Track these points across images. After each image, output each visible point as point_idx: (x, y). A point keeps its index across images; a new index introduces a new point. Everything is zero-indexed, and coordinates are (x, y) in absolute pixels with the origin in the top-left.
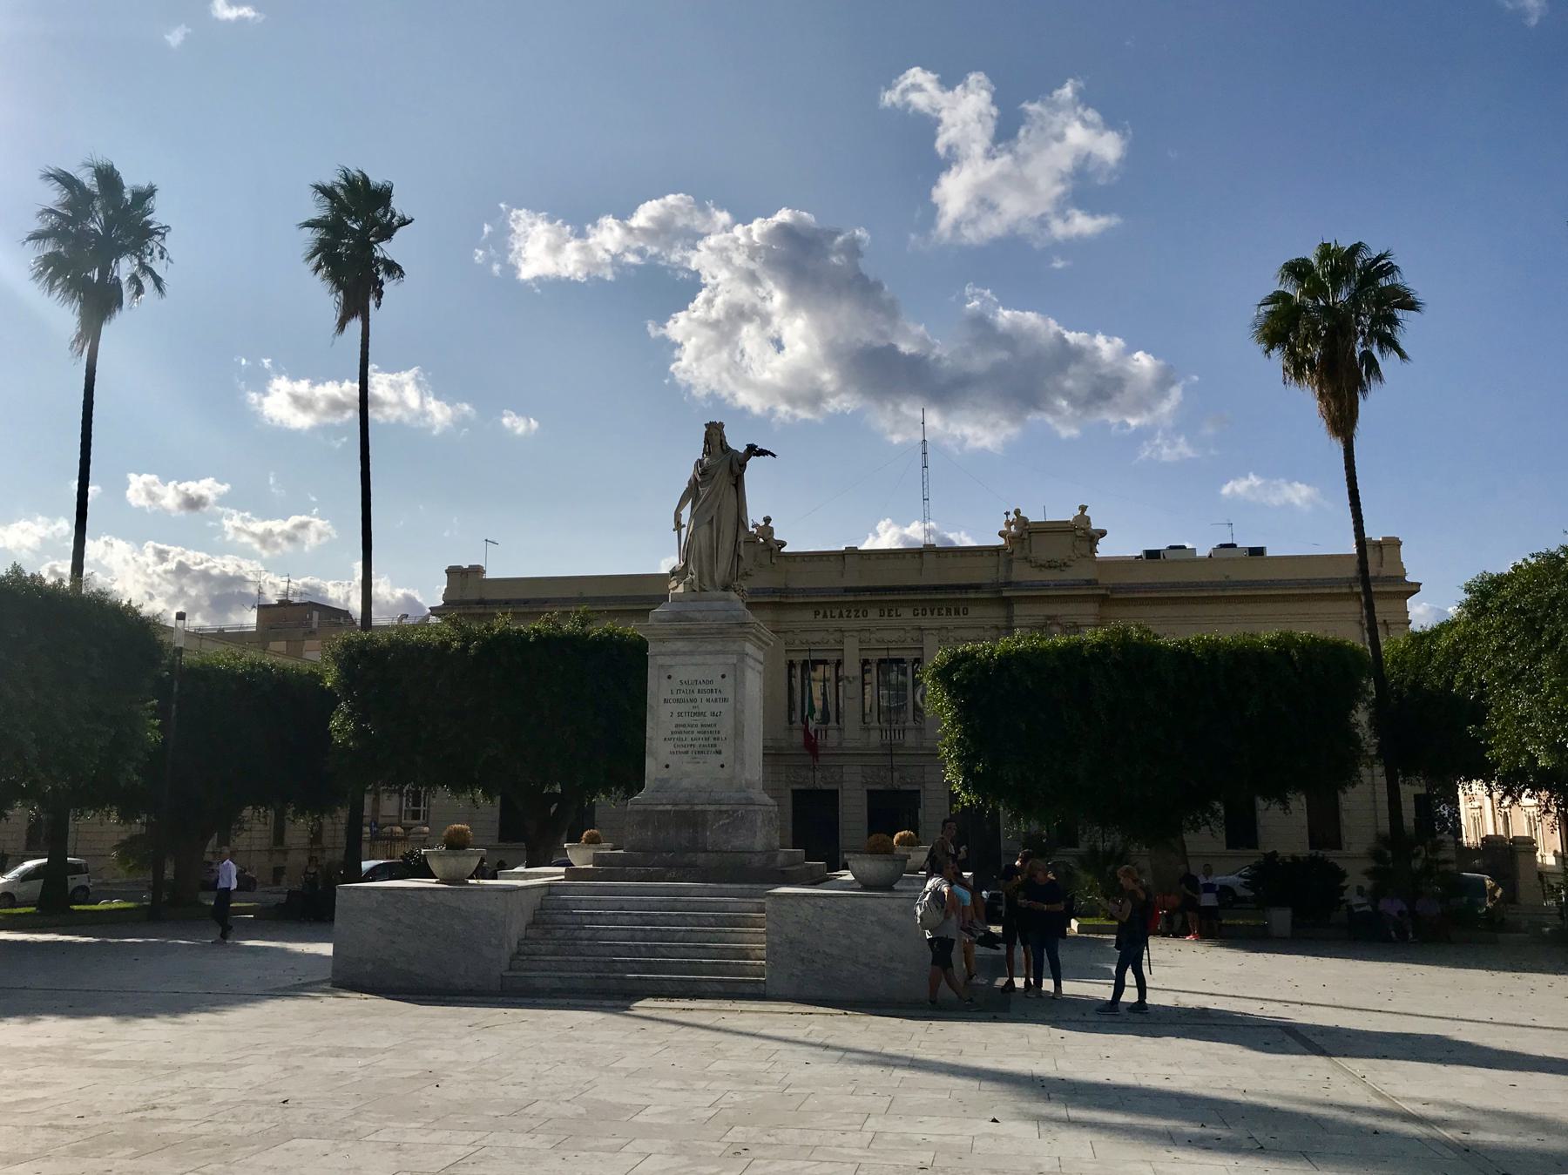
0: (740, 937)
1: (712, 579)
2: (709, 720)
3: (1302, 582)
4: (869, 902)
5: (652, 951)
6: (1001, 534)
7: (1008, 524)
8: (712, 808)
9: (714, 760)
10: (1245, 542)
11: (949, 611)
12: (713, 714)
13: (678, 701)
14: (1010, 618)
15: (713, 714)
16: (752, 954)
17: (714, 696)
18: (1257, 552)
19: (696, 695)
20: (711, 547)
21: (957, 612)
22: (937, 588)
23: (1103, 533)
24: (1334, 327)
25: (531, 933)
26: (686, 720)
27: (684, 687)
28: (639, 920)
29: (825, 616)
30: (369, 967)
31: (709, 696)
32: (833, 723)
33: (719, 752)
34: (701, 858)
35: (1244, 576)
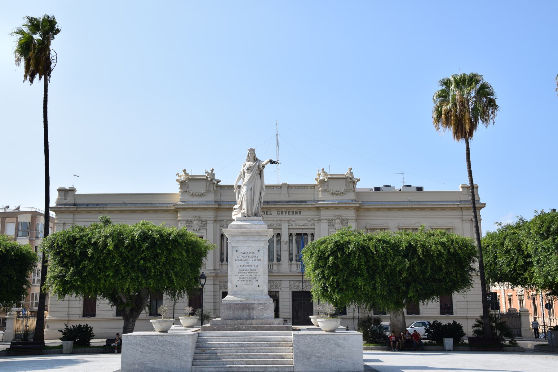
0: (281, 351)
1: (252, 211)
2: (253, 268)
3: (440, 203)
5: (247, 357)
6: (316, 179)
8: (256, 302)
9: (256, 284)
10: (415, 184)
11: (293, 212)
12: (255, 266)
13: (240, 260)
15: (255, 266)
16: (285, 357)
18: (420, 189)
19: (248, 258)
20: (251, 199)
21: (296, 213)
22: (288, 202)
23: (358, 180)
24: (466, 108)
25: (197, 351)
26: (244, 268)
27: (243, 255)
28: (238, 346)
29: (267, 214)
30: (137, 366)
33: (257, 281)
34: (253, 322)
35: (416, 200)
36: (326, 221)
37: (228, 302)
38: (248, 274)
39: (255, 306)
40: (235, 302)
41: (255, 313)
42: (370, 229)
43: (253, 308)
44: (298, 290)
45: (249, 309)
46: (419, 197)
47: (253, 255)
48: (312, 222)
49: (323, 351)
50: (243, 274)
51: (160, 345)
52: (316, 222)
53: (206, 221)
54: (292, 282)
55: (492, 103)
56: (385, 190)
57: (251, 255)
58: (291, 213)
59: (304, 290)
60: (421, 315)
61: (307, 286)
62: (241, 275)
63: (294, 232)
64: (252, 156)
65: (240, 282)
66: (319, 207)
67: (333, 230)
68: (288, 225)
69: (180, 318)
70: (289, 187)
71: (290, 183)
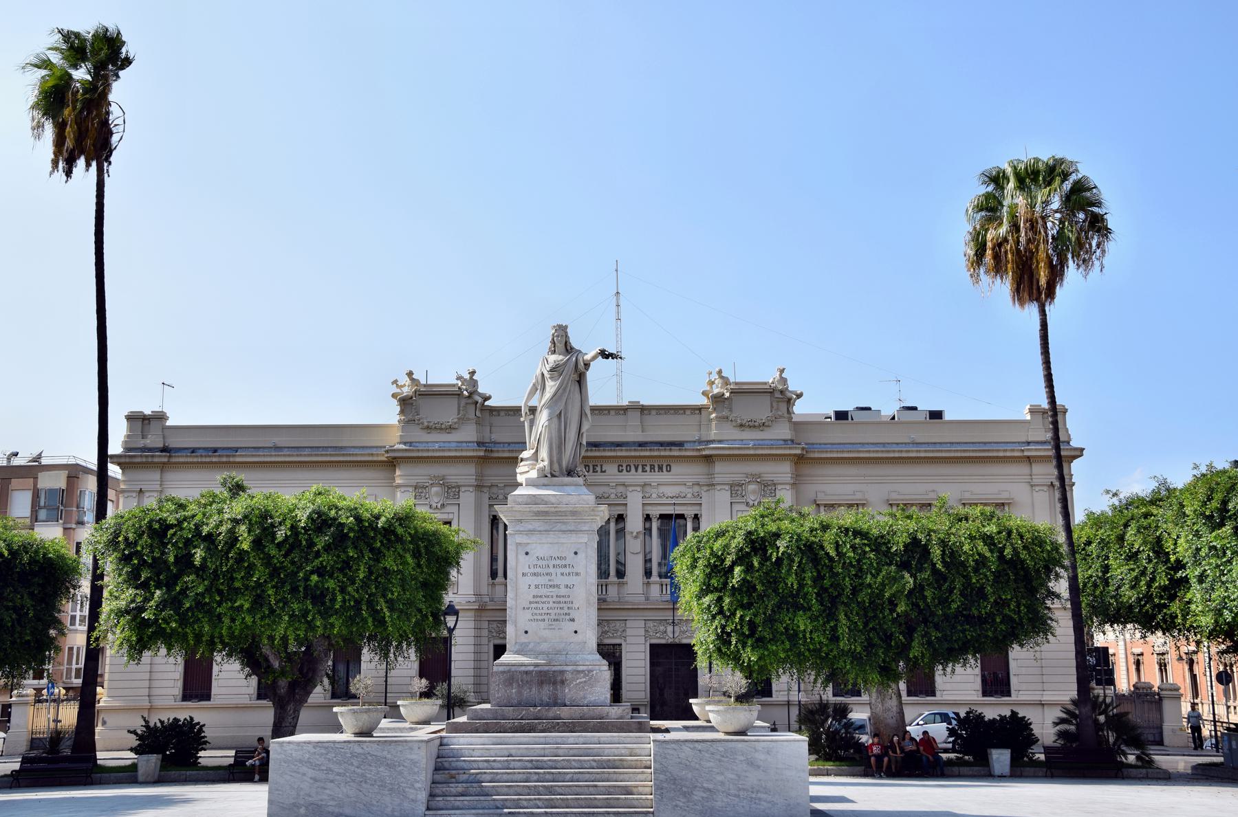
2: (563, 591)
3: (980, 449)
4: (740, 745)
5: (550, 791)
6: (704, 393)
7: (712, 383)
8: (569, 668)
11: (652, 467)
14: (711, 475)
16: (635, 790)
18: (936, 415)
19: (551, 570)
20: (560, 437)
21: (660, 469)
23: (799, 396)
24: (1038, 235)
25: (438, 777)
26: (543, 591)
27: (540, 563)
28: (529, 765)
31: (564, 570)
32: (500, 579)
33: (573, 620)
34: (564, 712)
35: (929, 441)
36: (727, 487)
37: (506, 668)
38: (551, 605)
39: (568, 676)
40: (523, 668)
41: (569, 693)
42: (825, 505)
43: (563, 682)
44: (663, 641)
45: (555, 683)
46: (934, 433)
47: (563, 562)
48: (696, 489)
49: (720, 778)
50: (540, 606)
51: (355, 763)
52: (705, 488)
53: (459, 487)
54: (651, 624)
56: (858, 417)
57: (558, 562)
58: (648, 468)
59: (677, 641)
60: (938, 697)
61: (684, 632)
63: (655, 512)
64: (562, 341)
65: (534, 624)
66: (710, 456)
67: (743, 507)
68: (641, 495)
69: (399, 703)
70: (644, 410)
71: (645, 402)
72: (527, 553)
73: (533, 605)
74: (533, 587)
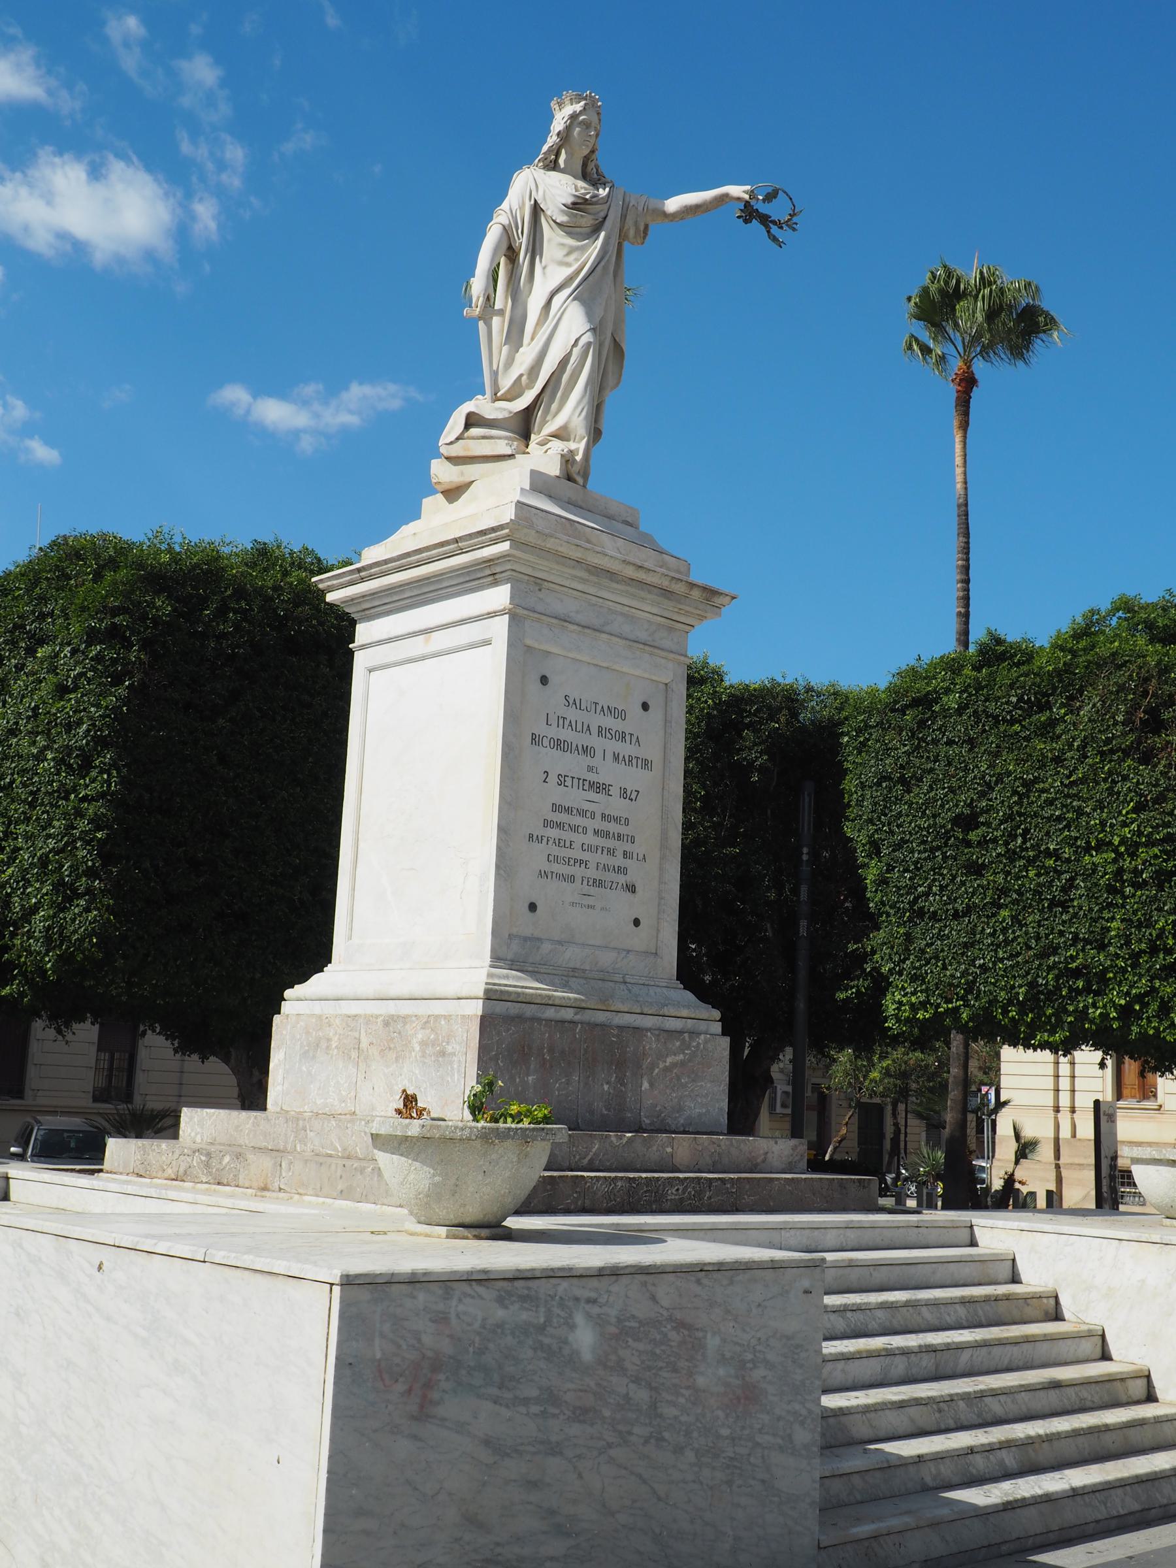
2: (617, 806)
12: (624, 793)
13: (559, 744)
15: (624, 793)
17: (625, 749)
26: (576, 797)
27: (572, 714)
33: (632, 889)
39: (651, 1044)
40: (550, 1013)
50: (567, 836)
55: (1055, 322)
57: (608, 722)
62: (558, 843)
72: (544, 680)
73: (554, 833)
74: (552, 779)
